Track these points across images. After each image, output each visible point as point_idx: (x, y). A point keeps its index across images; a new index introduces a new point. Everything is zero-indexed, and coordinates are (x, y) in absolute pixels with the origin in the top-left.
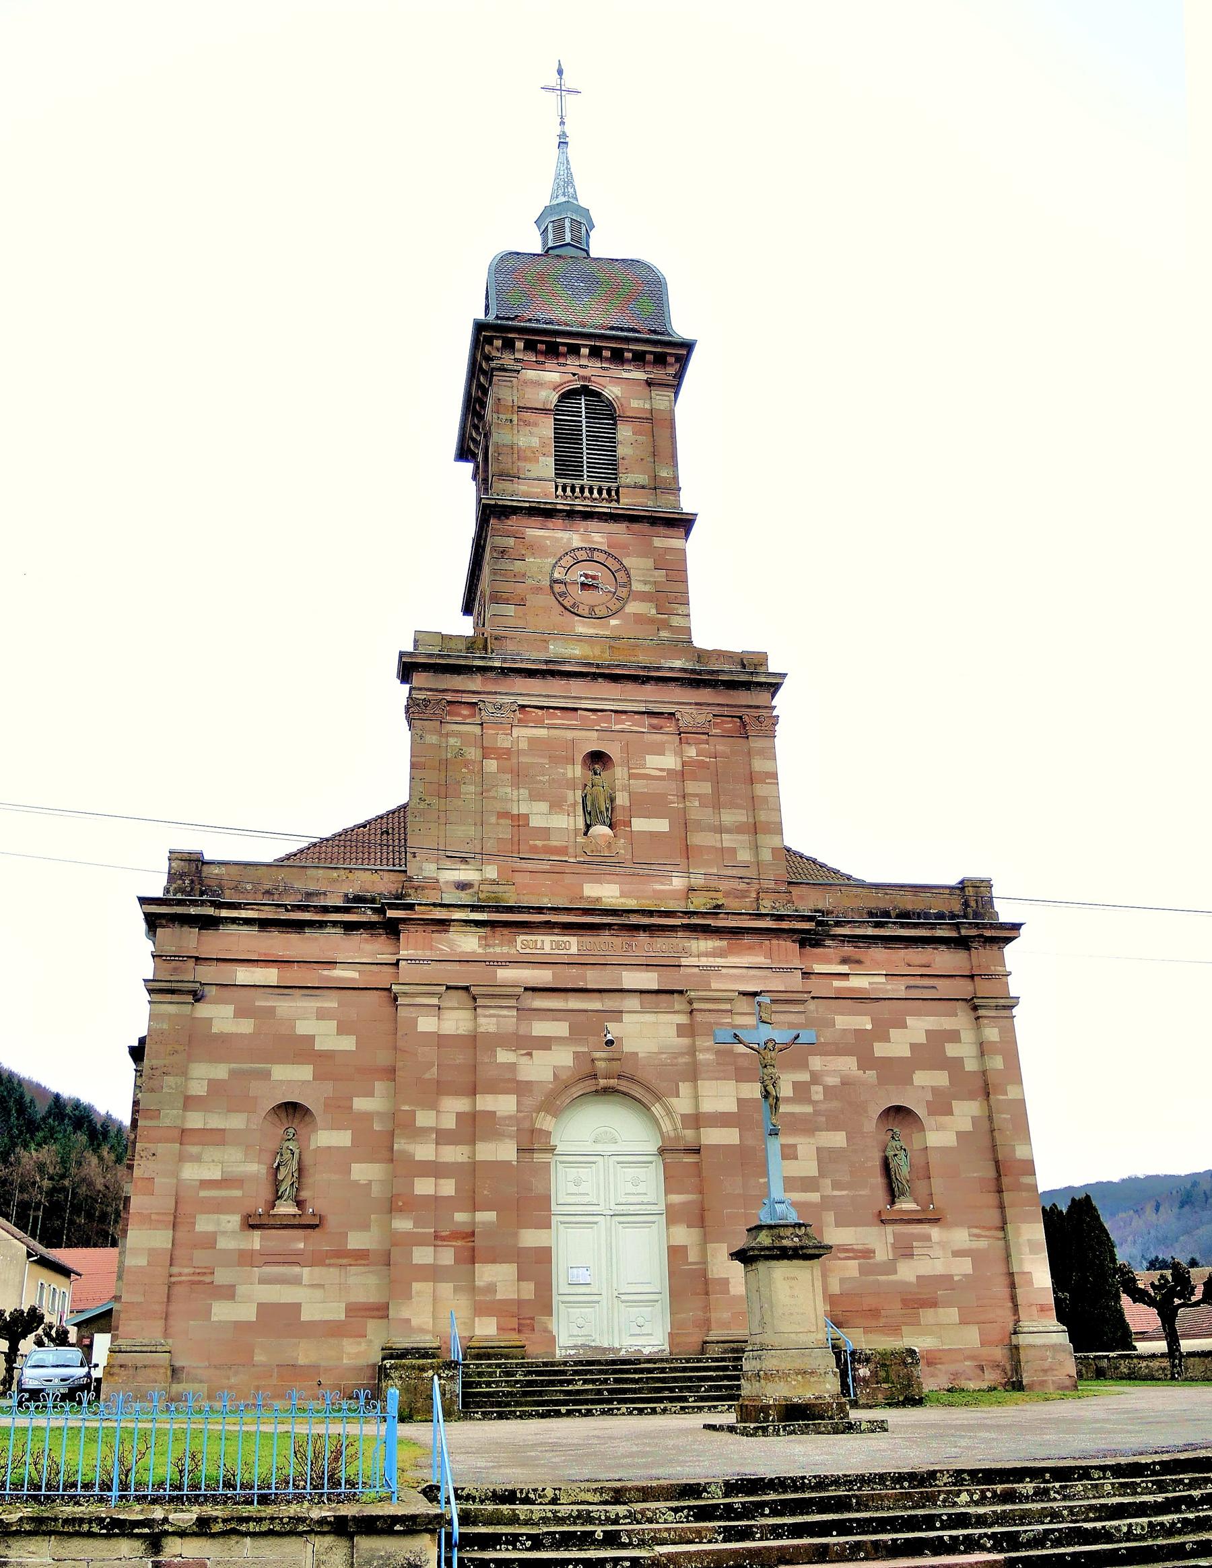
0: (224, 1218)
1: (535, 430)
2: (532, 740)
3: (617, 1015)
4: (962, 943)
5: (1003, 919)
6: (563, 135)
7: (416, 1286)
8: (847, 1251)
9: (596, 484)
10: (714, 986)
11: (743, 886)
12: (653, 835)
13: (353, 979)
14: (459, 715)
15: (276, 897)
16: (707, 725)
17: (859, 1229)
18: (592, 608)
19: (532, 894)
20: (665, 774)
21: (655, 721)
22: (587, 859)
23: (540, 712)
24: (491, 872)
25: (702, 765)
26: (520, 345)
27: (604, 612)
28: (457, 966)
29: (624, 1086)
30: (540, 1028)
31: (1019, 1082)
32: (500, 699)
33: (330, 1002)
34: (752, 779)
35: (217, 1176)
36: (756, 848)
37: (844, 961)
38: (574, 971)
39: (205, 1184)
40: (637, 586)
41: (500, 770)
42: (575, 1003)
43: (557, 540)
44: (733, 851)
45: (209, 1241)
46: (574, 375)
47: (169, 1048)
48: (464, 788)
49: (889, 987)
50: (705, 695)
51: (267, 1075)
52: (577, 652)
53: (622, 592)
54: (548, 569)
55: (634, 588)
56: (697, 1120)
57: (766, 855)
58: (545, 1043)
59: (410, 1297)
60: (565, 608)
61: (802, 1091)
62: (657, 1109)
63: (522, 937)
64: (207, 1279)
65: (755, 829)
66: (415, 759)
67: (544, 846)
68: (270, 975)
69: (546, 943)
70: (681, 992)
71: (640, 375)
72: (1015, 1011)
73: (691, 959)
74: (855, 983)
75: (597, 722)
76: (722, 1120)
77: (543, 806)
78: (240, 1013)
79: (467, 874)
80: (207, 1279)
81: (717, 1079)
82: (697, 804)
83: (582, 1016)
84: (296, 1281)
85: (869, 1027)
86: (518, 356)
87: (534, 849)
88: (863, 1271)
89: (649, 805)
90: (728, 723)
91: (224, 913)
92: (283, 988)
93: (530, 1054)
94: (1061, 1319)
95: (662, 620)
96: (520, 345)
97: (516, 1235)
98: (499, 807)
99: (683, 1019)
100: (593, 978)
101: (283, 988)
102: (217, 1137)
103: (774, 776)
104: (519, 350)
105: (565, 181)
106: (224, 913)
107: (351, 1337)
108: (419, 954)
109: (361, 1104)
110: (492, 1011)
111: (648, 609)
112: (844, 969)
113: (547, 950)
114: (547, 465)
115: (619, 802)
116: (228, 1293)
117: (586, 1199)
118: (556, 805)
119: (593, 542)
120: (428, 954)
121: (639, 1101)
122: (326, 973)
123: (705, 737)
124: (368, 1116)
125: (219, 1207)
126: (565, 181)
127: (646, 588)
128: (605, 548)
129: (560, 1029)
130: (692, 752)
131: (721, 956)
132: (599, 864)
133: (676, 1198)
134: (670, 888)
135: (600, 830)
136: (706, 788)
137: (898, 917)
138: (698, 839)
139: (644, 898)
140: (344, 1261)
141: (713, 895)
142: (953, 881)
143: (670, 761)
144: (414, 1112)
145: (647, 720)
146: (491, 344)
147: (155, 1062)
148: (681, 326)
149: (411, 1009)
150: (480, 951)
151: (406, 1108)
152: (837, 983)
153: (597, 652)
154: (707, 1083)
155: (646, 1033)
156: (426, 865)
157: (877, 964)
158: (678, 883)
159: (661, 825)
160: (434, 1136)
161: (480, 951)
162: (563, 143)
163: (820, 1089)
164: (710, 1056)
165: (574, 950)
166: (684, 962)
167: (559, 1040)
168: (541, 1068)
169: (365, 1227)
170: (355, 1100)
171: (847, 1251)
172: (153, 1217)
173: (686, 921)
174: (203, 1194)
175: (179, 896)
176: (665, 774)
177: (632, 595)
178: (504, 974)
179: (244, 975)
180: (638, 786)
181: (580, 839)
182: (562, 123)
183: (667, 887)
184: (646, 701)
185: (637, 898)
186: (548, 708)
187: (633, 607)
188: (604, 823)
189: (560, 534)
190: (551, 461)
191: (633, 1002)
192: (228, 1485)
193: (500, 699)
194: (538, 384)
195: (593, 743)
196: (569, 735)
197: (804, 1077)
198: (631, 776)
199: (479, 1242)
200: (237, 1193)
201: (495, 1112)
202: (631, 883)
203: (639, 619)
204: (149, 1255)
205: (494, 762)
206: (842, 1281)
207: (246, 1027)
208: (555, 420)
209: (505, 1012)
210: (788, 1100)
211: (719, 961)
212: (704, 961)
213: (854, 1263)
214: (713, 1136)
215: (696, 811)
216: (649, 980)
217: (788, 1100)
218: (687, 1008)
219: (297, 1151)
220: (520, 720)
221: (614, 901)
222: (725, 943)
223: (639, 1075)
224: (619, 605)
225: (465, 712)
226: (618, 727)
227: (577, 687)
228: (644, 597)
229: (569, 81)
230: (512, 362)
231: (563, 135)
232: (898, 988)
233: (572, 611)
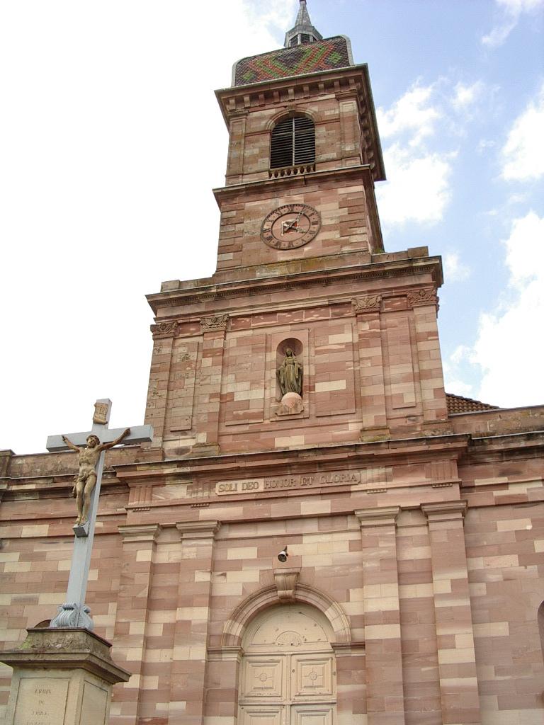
1: (257, 144)
2: (239, 340)
10: (380, 505)
11: (409, 423)
14: (189, 331)
16: (378, 305)
20: (343, 346)
21: (337, 311)
22: (278, 419)
23: (248, 320)
24: (202, 438)
25: (373, 335)
26: (247, 98)
27: (300, 243)
28: (168, 511)
29: (301, 595)
30: (234, 553)
32: (217, 315)
34: (414, 339)
37: (503, 474)
38: (260, 505)
40: (325, 222)
41: (214, 364)
42: (263, 531)
43: (267, 205)
44: (401, 396)
48: (187, 381)
51: (34, 601)
52: (277, 273)
54: (260, 224)
55: (323, 224)
56: (363, 620)
57: (429, 396)
58: (238, 565)
60: (272, 247)
62: (329, 613)
63: (220, 483)
65: (418, 377)
66: (153, 366)
67: (244, 414)
70: (352, 514)
74: (514, 490)
75: (291, 319)
76: (385, 618)
77: (246, 385)
78: (23, 558)
79: (186, 442)
81: (380, 583)
82: (369, 364)
83: (269, 541)
85: (529, 527)
86: (247, 105)
87: (237, 417)
89: (327, 372)
90: (397, 301)
91: (14, 488)
92: (51, 538)
93: (224, 575)
95: (344, 240)
96: (247, 98)
98: (211, 390)
99: (355, 536)
100: (276, 510)
101: (51, 538)
104: (247, 102)
105: (304, 14)
106: (14, 488)
108: (141, 504)
110: (194, 542)
111: (336, 235)
112: (504, 480)
113: (240, 491)
115: (306, 373)
117: (272, 692)
119: (294, 201)
120: (148, 503)
121: (315, 607)
123: (377, 315)
126: (304, 14)
127: (333, 222)
128: (303, 203)
129: (250, 552)
130: (366, 327)
131: (386, 480)
132: (289, 419)
133: (345, 688)
134: (349, 430)
136: (377, 351)
138: (368, 391)
143: (347, 337)
144: (129, 623)
145: (330, 311)
146: (228, 103)
149: (134, 545)
150: (188, 497)
151: (123, 620)
152: (497, 493)
154: (372, 587)
155: (320, 551)
157: (535, 473)
158: (353, 428)
159: (340, 385)
160: (142, 641)
161: (188, 497)
163: (483, 585)
164: (375, 564)
165: (261, 489)
166: (353, 488)
167: (249, 562)
168: (234, 586)
177: (321, 229)
178: (204, 513)
179: (27, 531)
180: (322, 359)
181: (274, 405)
183: (344, 432)
184: (328, 297)
186: (253, 315)
187: (322, 236)
188: (294, 391)
191: (312, 526)
195: (285, 333)
196: (269, 331)
198: (317, 352)
201: (190, 621)
202: (467, 482)
207: (26, 567)
209: (204, 542)
211: (383, 485)
212: (370, 486)
214: (375, 633)
215: (368, 370)
216: (324, 506)
218: (357, 526)
220: (232, 328)
222: (390, 470)
223: (316, 585)
224: (311, 236)
227: (275, 298)
228: (331, 228)
233: (278, 247)
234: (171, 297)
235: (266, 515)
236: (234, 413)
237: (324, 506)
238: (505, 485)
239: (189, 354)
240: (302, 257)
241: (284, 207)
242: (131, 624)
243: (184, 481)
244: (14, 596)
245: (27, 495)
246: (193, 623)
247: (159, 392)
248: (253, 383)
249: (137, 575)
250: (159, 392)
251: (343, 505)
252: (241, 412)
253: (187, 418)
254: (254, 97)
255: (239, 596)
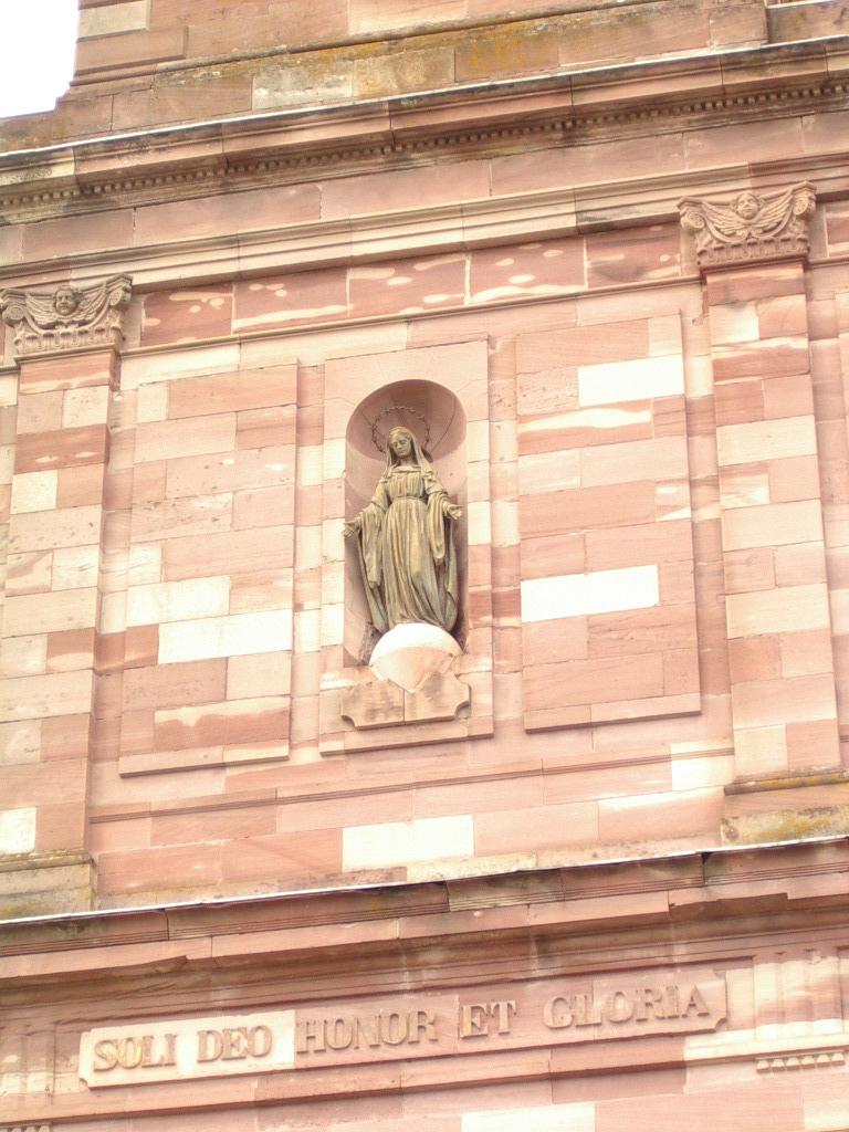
12: (599, 629)
16: (798, 230)
17: (16, 975)
20: (645, 416)
21: (615, 256)
22: (356, 741)
23: (216, 300)
63: (98, 1033)
77: (211, 592)
82: (761, 494)
87: (173, 736)
89: (572, 530)
113: (187, 1067)
115: (478, 534)
132: (405, 741)
135: (413, 638)
136: (793, 437)
143: (665, 372)
145: (586, 259)
159: (631, 589)
166: (693, 1049)
173: (687, 897)
180: (552, 473)
184: (576, 196)
186: (243, 279)
188: (427, 615)
192: (240, 344)
193: (79, 279)
196: (311, 350)
198: (527, 444)
220: (147, 336)
226: (485, 297)
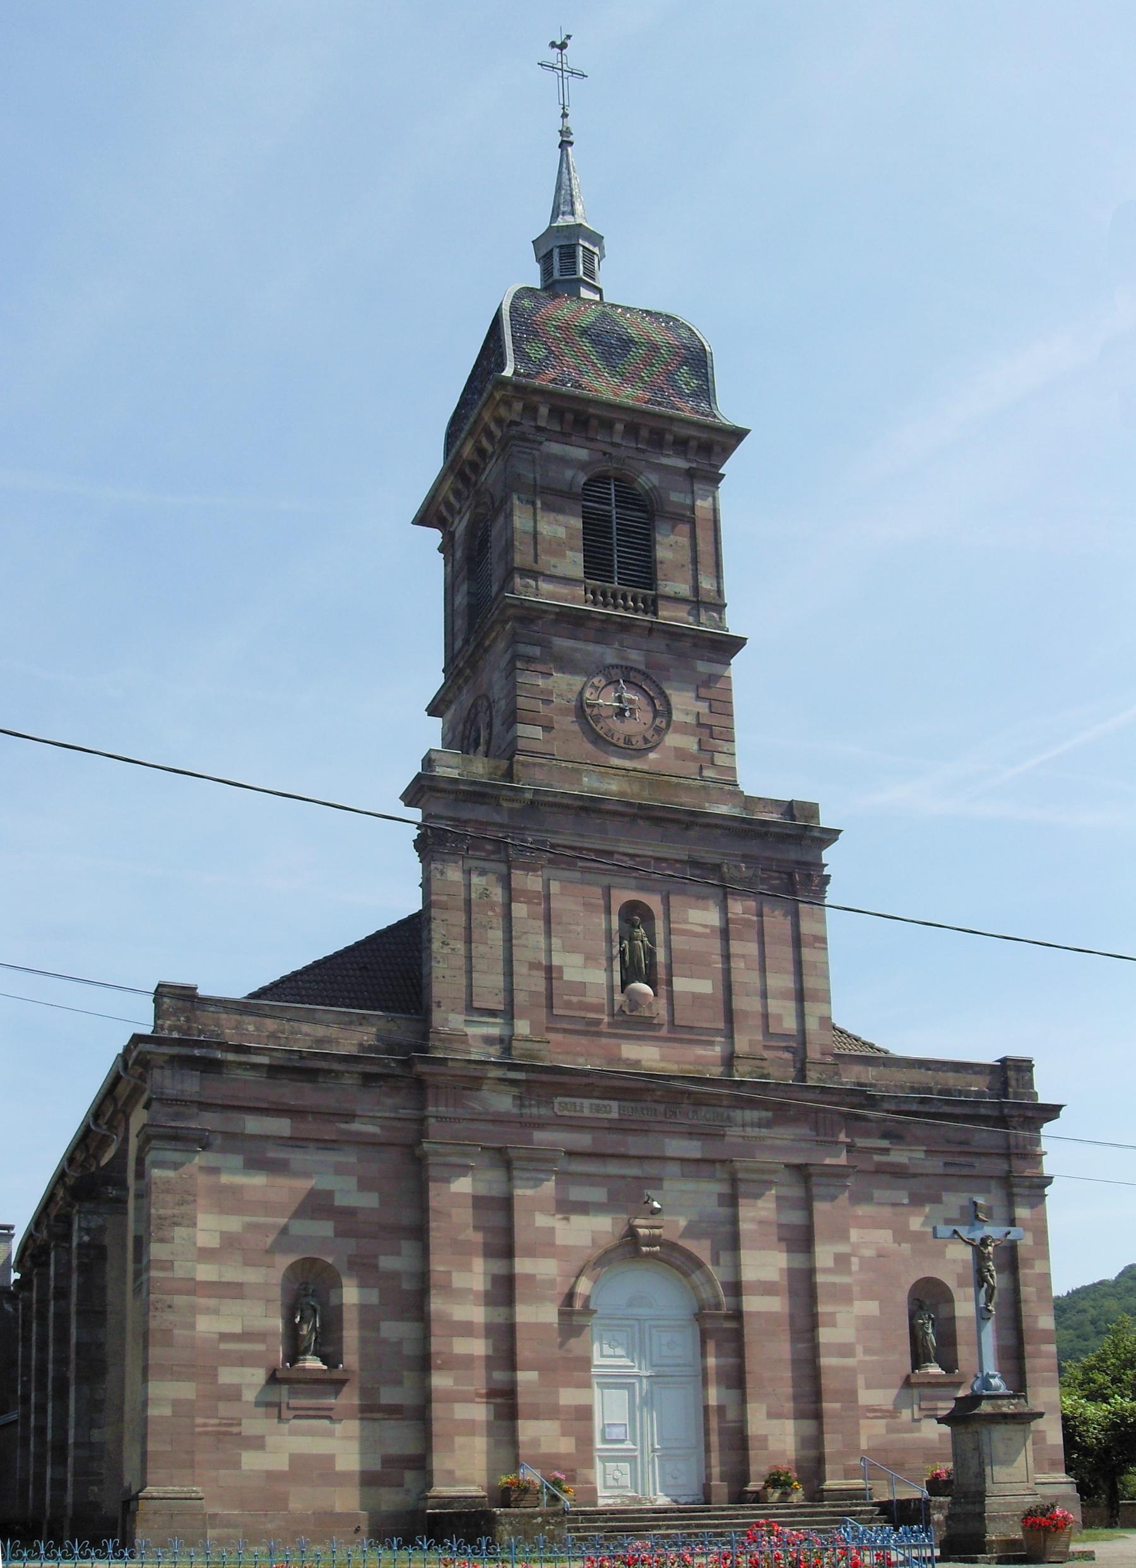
0: (248, 1371)
3: (656, 1182)
4: (1002, 1121)
5: (1042, 1100)
6: (565, 132)
7: (459, 1440)
8: (875, 1411)
9: (630, 591)
13: (374, 1135)
15: (282, 1042)
18: (628, 740)
19: (568, 1053)
20: (708, 931)
31: (1045, 1256)
33: (349, 1158)
35: (237, 1329)
36: (801, 1016)
39: (224, 1337)
40: (677, 716)
42: (612, 1168)
45: (234, 1394)
46: (605, 454)
47: (178, 1197)
49: (927, 1163)
50: (753, 847)
53: (661, 722)
55: (674, 718)
59: (453, 1451)
61: (842, 1261)
64: (235, 1430)
68: (281, 1126)
69: (586, 1107)
71: (682, 464)
72: (1047, 1190)
73: (734, 1129)
80: (235, 1430)
82: (742, 965)
84: (330, 1434)
88: (890, 1430)
90: (776, 879)
93: (567, 1219)
94: (1068, 1470)
96: (619, 427)
97: (557, 1393)
102: (234, 1291)
103: (824, 940)
107: (391, 1486)
109: (387, 1263)
111: (690, 743)
112: (885, 1143)
113: (586, 1113)
114: (573, 563)
116: (257, 1443)
118: (590, 959)
122: (343, 1126)
124: (396, 1275)
125: (243, 1360)
128: (642, 667)
129: (598, 1194)
132: (632, 1022)
137: (940, 1093)
139: (684, 1063)
140: (378, 1415)
141: (758, 1063)
142: (990, 1057)
144: (449, 1273)
147: (162, 1212)
148: (729, 409)
151: (441, 1268)
153: (636, 788)
156: (452, 1017)
162: (564, 145)
165: (615, 1115)
169: (399, 1383)
170: (382, 1258)
171: (875, 1411)
172: (175, 1368)
174: (223, 1346)
175: (175, 1035)
176: (708, 931)
179: (254, 1125)
182: (565, 116)
185: (677, 1063)
187: (672, 740)
189: (590, 647)
190: (580, 557)
194: (563, 461)
197: (843, 1248)
199: (522, 1400)
200: (261, 1347)
203: (681, 754)
204: (173, 1406)
205: (524, 907)
206: (869, 1438)
208: (583, 506)
210: (827, 1271)
213: (883, 1422)
217: (827, 1271)
219: (318, 1307)
221: (654, 1065)
225: (489, 847)
228: (684, 729)
229: (573, 56)
230: (533, 431)
231: (565, 132)
232: (935, 1165)
234: (461, 787)
235: (622, 1150)
236: (566, 997)
237: (692, 1149)
238: (885, 1151)
239: (490, 889)
240: (645, 767)
241: (617, 666)
242: (454, 1274)
243: (508, 1088)
244: (247, 1219)
245: (245, 1069)
246: (538, 1277)
247: (452, 942)
248: (588, 958)
249: (454, 1211)
250: (452, 942)
251: (714, 1150)
252: (575, 999)
253: (497, 991)
254: (556, 412)
255: (588, 1247)
